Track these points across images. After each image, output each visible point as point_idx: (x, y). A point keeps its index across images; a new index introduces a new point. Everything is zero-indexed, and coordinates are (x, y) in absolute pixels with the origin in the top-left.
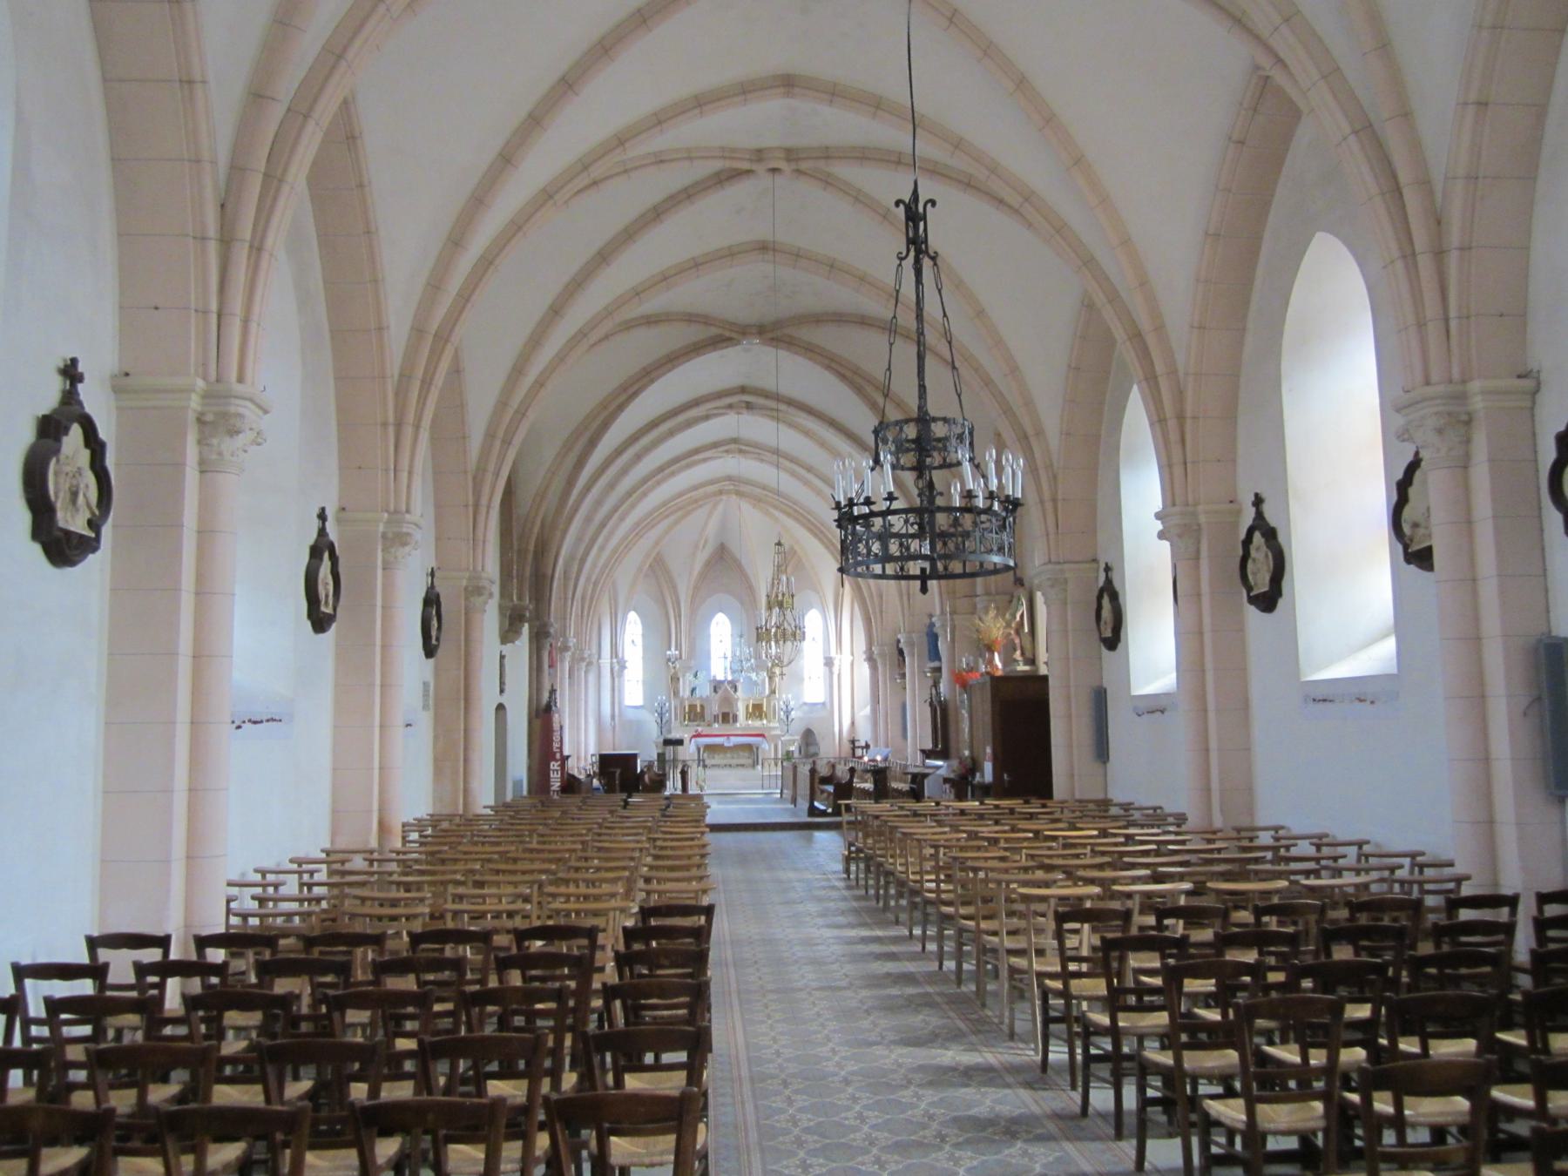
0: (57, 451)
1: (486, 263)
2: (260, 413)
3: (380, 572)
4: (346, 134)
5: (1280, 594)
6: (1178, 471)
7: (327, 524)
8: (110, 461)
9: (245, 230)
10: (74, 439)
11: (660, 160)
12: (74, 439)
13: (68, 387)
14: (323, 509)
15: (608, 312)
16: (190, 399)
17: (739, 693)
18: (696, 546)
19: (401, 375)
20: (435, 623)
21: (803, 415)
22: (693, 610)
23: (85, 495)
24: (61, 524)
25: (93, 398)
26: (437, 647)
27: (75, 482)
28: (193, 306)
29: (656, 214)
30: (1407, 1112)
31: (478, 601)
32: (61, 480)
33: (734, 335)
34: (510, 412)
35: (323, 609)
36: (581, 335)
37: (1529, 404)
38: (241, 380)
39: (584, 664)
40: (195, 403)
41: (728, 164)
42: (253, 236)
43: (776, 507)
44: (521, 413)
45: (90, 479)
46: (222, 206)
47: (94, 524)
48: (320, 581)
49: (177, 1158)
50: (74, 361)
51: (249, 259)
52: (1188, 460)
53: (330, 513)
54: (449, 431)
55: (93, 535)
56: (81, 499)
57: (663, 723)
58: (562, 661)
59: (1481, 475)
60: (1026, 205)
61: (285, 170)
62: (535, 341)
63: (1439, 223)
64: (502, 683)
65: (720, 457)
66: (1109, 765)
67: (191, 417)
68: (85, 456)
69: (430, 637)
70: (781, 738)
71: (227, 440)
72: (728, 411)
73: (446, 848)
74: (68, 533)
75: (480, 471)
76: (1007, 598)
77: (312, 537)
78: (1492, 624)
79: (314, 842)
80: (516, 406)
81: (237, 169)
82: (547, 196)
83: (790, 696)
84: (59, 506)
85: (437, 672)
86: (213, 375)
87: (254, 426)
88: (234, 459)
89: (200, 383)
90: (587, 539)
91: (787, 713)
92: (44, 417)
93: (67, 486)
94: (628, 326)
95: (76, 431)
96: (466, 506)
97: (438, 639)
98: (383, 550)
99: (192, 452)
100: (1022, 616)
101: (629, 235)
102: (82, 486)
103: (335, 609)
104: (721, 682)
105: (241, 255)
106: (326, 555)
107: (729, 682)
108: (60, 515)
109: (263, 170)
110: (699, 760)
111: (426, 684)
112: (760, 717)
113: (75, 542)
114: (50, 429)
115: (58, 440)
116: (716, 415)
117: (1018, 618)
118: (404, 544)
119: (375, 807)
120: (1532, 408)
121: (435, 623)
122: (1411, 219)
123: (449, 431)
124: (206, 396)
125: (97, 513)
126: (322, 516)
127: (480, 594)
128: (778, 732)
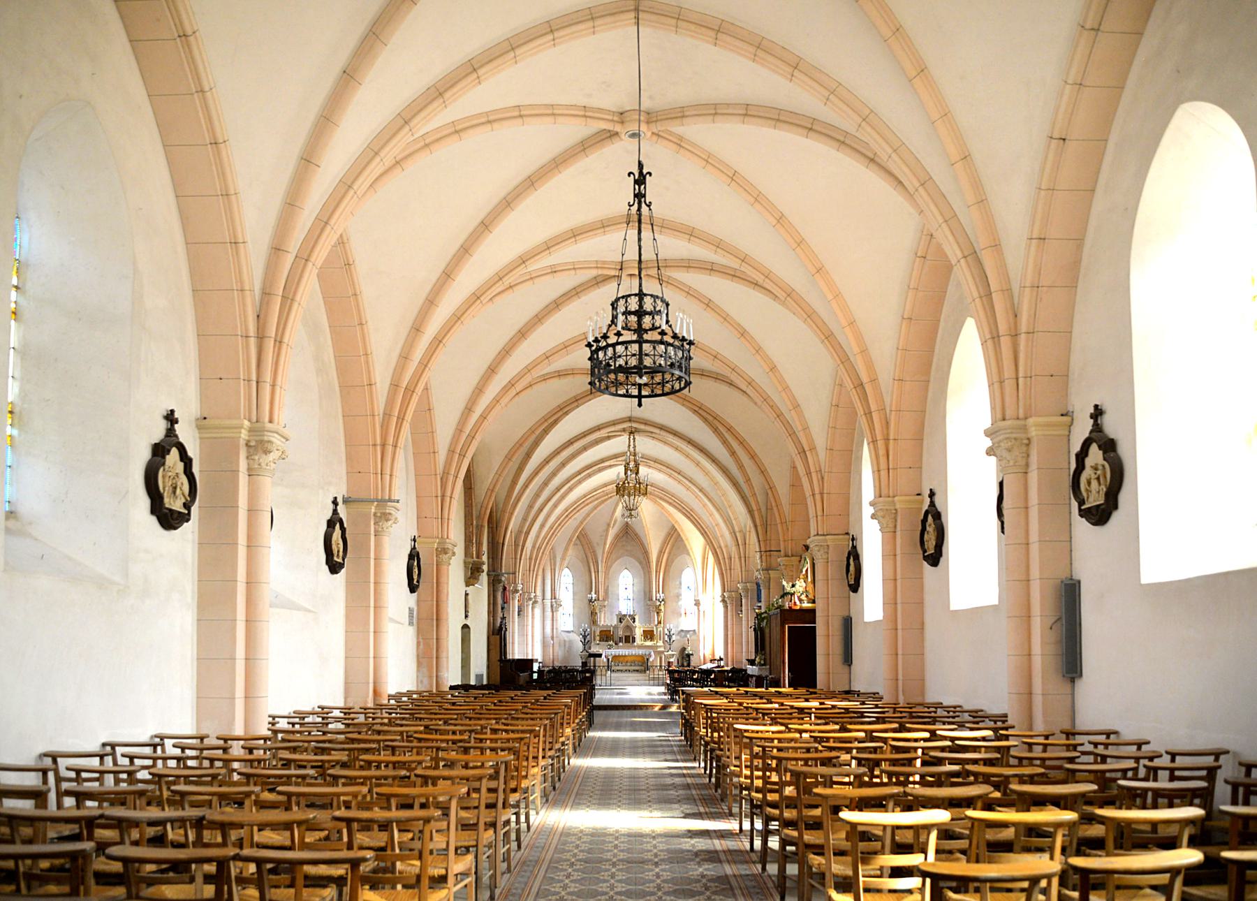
0: (164, 464)
1: (438, 341)
2: (284, 440)
3: (372, 538)
4: (342, 262)
5: (941, 555)
6: (884, 473)
7: (338, 507)
8: (196, 469)
9: (272, 331)
10: (173, 456)
11: (554, 271)
12: (173, 456)
13: (169, 426)
14: (336, 498)
15: (528, 369)
16: (240, 433)
17: (637, 623)
18: (609, 525)
19: (385, 414)
20: (416, 570)
21: (671, 436)
22: (608, 568)
23: (181, 489)
24: (167, 506)
25: (185, 433)
26: (418, 586)
27: (174, 481)
28: (242, 377)
29: (556, 305)
30: (897, 838)
31: (445, 557)
32: (167, 479)
33: (684, 369)
34: (464, 436)
35: (335, 559)
36: (511, 384)
37: (1067, 433)
38: (271, 421)
39: (531, 602)
40: (244, 435)
41: (600, 272)
42: (276, 335)
43: (661, 498)
44: (471, 437)
45: (184, 479)
46: (258, 316)
47: (187, 506)
48: (333, 542)
49: (269, 891)
50: (172, 411)
51: (274, 347)
52: (891, 467)
53: (340, 500)
54: (425, 446)
55: (186, 512)
56: (178, 491)
57: (586, 643)
58: (513, 599)
59: (1033, 476)
60: (788, 299)
61: (295, 293)
62: (479, 390)
63: (1016, 316)
64: (466, 611)
65: (620, 435)
66: (852, 667)
67: (242, 443)
68: (181, 466)
69: (413, 579)
70: (663, 655)
71: (264, 456)
72: (623, 433)
73: (441, 723)
74: (171, 510)
75: (446, 473)
76: (798, 558)
77: (329, 515)
78: (1035, 573)
79: (335, 698)
80: (468, 432)
81: (266, 294)
82: (476, 297)
83: (672, 626)
84: (165, 495)
85: (418, 602)
86: (254, 419)
87: (280, 448)
88: (268, 468)
89: (246, 423)
90: (530, 519)
91: (670, 637)
92: (155, 444)
93: (170, 483)
94: (545, 378)
95: (174, 452)
96: (437, 497)
97: (418, 582)
98: (374, 524)
99: (243, 465)
100: (807, 570)
101: (539, 319)
102: (179, 484)
103: (343, 560)
104: (625, 616)
105: (270, 345)
106: (338, 526)
107: (630, 616)
108: (166, 500)
109: (281, 294)
110: (608, 666)
111: (411, 610)
112: (652, 639)
113: (175, 516)
114: (159, 451)
115: (164, 457)
116: (615, 436)
117: (804, 572)
118: (387, 520)
119: (371, 680)
120: (1069, 436)
121: (416, 570)
122: (998, 315)
123: (425, 446)
124: (250, 430)
125: (189, 499)
126: (335, 502)
127: (446, 553)
128: (662, 649)
